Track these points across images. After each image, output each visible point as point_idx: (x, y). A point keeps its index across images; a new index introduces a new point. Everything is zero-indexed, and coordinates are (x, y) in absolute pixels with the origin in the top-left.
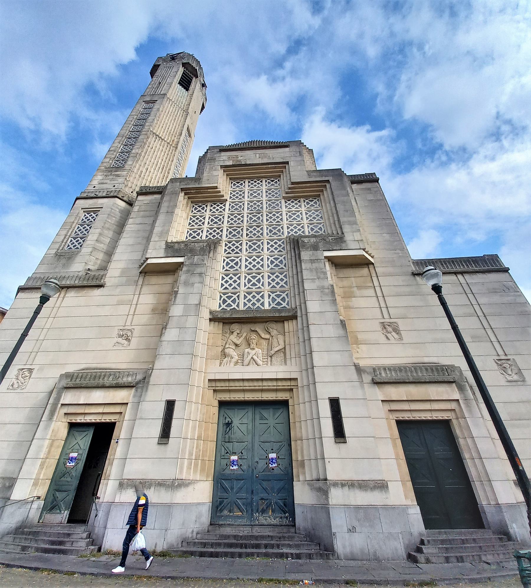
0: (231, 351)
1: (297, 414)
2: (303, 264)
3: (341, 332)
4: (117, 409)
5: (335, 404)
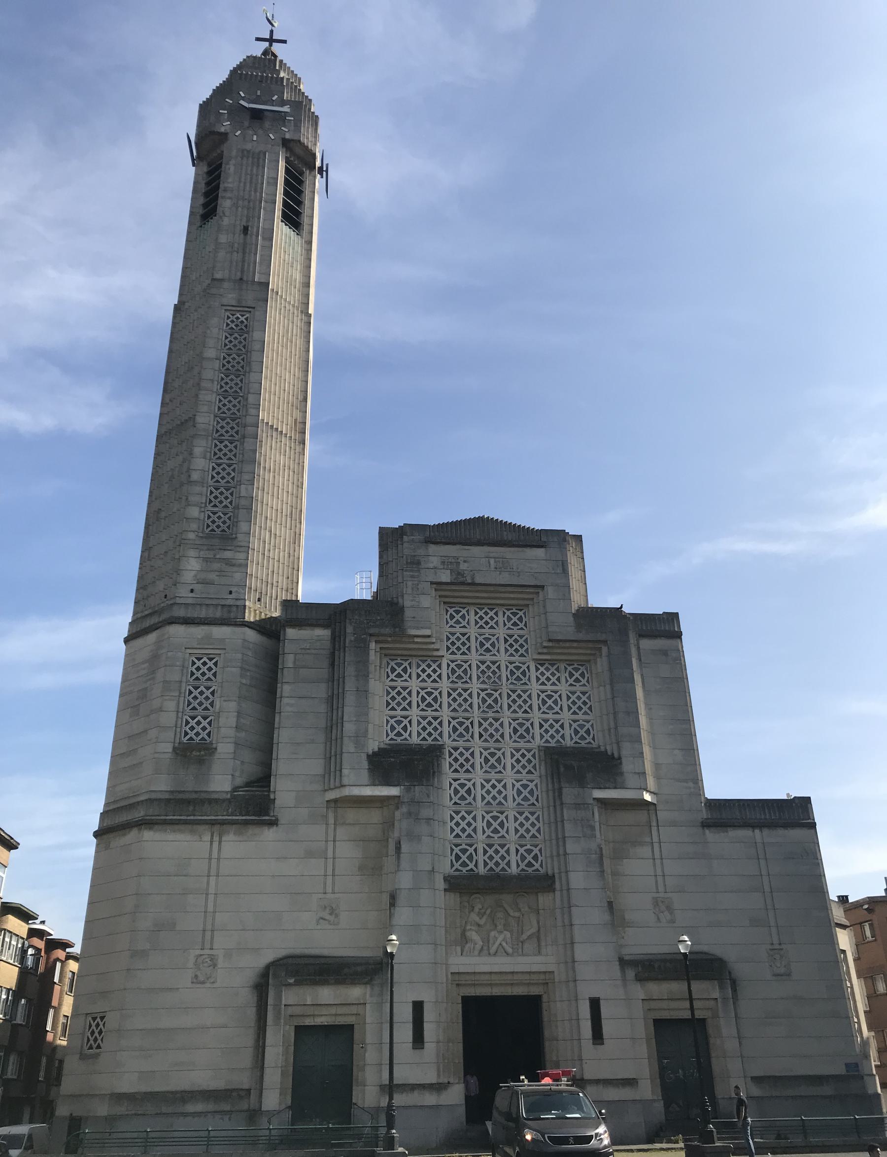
0: (474, 935)
2: (565, 811)
3: (607, 917)
4: (354, 1009)
5: (595, 1004)
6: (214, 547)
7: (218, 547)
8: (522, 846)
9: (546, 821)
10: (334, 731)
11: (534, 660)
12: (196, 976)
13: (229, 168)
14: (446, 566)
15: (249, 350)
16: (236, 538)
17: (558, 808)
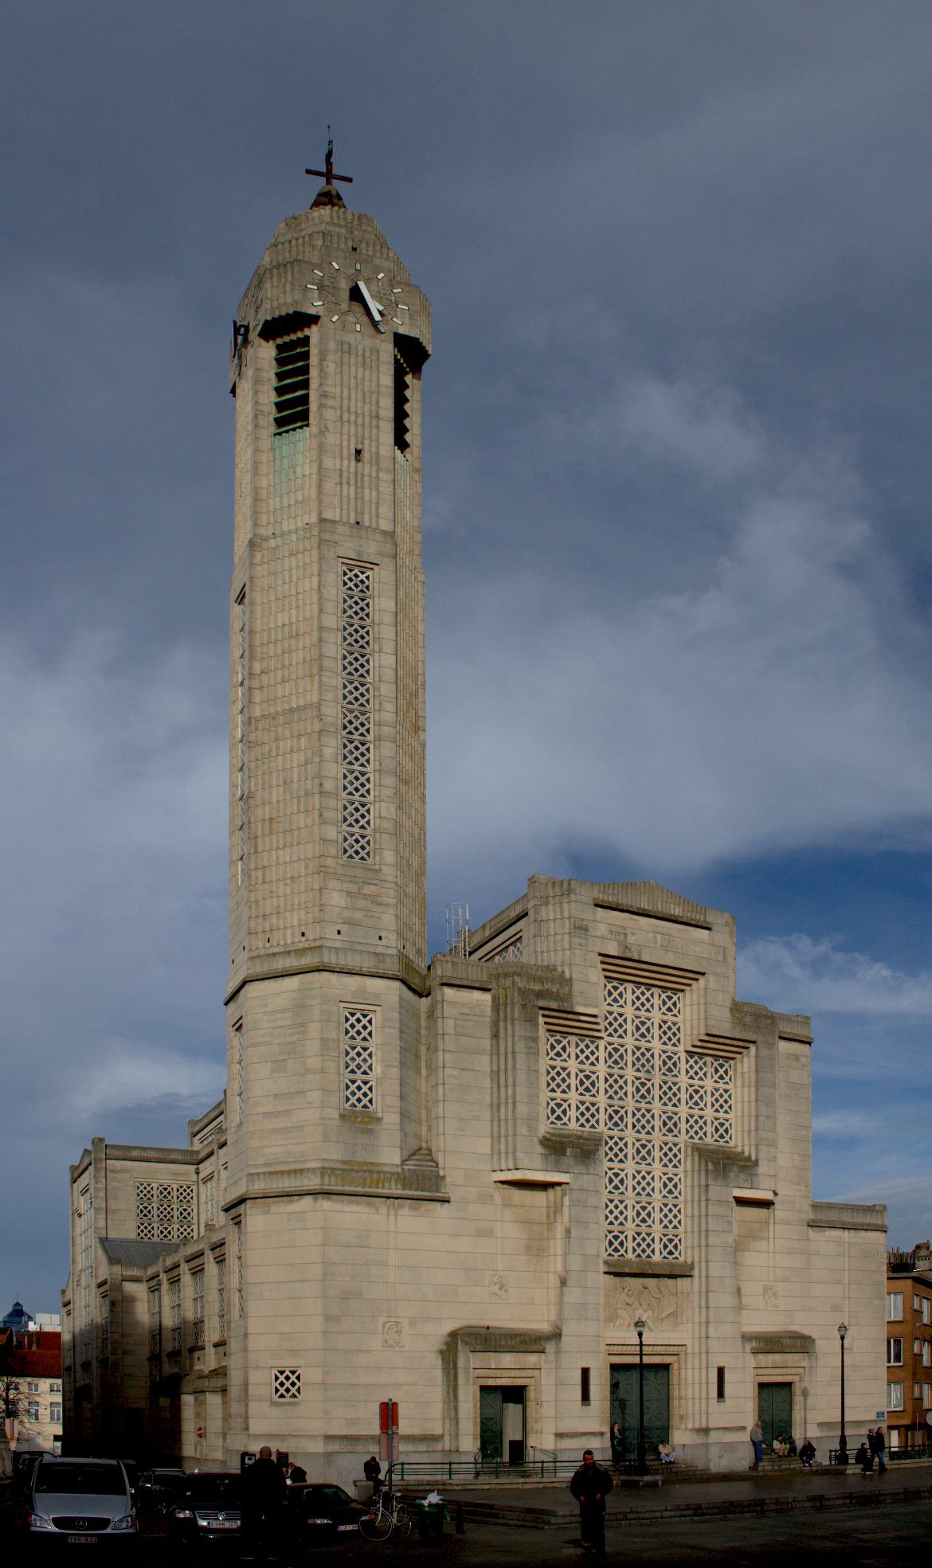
1: (683, 1376)
2: (710, 1207)
6: (358, 880)
7: (362, 880)
8: (665, 1235)
9: (689, 1214)
10: (503, 1110)
11: (687, 1052)
12: (386, 1341)
13: (327, 367)
14: (613, 937)
15: (376, 621)
16: (380, 869)
17: (703, 1203)
